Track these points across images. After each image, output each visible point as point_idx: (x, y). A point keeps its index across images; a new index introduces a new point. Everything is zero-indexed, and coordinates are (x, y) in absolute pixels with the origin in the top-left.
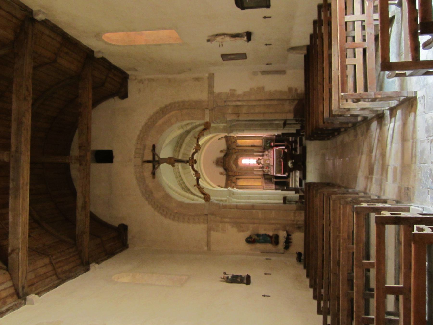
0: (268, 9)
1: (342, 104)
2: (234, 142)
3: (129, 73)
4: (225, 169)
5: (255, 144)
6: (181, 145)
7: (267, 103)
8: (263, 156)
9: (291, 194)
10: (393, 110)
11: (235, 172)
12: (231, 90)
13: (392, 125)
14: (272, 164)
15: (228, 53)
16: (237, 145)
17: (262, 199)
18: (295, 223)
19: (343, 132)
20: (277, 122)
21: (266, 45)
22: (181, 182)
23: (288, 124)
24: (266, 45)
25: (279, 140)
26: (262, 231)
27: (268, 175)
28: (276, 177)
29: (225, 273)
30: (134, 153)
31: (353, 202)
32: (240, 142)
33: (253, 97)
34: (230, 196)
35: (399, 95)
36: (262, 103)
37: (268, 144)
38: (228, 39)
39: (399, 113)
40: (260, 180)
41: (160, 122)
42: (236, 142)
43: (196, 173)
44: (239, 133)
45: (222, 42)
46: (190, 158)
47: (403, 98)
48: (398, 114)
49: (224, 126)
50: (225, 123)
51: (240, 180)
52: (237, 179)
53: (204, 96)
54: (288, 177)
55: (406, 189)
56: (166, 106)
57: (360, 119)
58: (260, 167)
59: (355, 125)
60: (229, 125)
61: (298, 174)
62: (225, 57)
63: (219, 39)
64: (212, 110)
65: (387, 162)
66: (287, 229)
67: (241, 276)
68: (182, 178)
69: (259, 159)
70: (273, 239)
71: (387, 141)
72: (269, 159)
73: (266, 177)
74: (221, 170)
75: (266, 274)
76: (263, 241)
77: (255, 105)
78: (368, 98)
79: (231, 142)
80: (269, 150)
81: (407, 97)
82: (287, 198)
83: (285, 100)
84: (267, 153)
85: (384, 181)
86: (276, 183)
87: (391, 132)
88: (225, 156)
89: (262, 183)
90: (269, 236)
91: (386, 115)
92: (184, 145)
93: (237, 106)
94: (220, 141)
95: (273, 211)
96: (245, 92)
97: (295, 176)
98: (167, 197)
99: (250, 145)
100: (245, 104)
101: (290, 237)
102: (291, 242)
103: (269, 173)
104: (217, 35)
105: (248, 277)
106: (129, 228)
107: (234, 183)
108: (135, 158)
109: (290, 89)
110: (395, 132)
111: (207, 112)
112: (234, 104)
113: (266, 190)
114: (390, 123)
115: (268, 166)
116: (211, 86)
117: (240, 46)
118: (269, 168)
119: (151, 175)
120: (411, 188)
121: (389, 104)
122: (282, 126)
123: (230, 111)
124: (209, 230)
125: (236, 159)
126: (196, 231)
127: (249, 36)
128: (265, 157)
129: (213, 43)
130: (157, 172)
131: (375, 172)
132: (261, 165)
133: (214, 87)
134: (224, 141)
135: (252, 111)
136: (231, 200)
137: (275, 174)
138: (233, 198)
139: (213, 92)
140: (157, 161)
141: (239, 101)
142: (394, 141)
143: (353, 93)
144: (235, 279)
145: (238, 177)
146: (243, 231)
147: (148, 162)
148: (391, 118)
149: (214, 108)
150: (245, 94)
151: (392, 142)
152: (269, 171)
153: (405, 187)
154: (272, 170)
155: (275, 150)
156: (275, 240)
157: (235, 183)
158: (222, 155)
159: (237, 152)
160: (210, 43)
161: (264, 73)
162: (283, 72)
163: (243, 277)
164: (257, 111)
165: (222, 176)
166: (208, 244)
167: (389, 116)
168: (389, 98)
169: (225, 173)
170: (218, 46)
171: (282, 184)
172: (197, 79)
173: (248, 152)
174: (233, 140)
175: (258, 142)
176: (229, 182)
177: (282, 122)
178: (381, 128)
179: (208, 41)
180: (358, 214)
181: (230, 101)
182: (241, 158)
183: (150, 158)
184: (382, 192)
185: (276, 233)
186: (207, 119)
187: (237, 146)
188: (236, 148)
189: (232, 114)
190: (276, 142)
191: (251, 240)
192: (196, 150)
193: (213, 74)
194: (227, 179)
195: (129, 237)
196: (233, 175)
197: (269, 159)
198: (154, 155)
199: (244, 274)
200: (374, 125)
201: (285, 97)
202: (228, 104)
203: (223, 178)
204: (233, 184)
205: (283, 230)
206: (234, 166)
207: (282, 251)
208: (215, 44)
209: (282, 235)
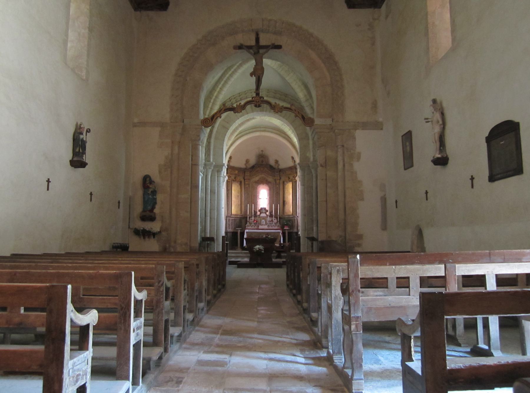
0: (487, 178)
1: (338, 271)
2: (289, 178)
3: (384, 6)
4: (253, 167)
5: (286, 206)
7: (341, 206)
8: (271, 216)
9: (218, 247)
10: (329, 360)
11: (249, 179)
12: (359, 154)
13: (303, 360)
14: (260, 227)
15: (413, 143)
16: (286, 183)
18: (172, 244)
19: (297, 299)
20: (315, 228)
21: (427, 193)
23: (312, 244)
24: (427, 193)
25: (292, 237)
26: (159, 197)
27: (246, 223)
28: (242, 234)
29: (88, 131)
30: (269, 18)
31: (160, 287)
32: (290, 186)
34: (215, 166)
35: (355, 365)
37: (287, 223)
38: (437, 129)
39: (321, 370)
40: (239, 213)
41: (313, 55)
42: (290, 181)
43: (243, 107)
44: (300, 183)
45: (432, 121)
46: (263, 98)
47: (350, 374)
48: (320, 368)
50: (314, 158)
51: (239, 187)
53: (351, 115)
54: (243, 248)
55: (180, 380)
56: (336, 63)
57: (314, 315)
58: (255, 213)
59: (306, 311)
60: (311, 165)
61: (247, 260)
62: (408, 137)
63: (438, 116)
64: (331, 128)
65: (238, 353)
66: (163, 233)
67: (84, 153)
69: (267, 211)
70: (148, 214)
71: (275, 353)
72: (266, 224)
73: (243, 221)
75: (91, 194)
76: (146, 199)
77: (337, 188)
78: (349, 310)
79: (290, 174)
80: (278, 224)
81: (352, 379)
82: (212, 243)
83: (345, 230)
84: (275, 221)
85: (206, 349)
86: (234, 234)
87: (289, 358)
88: (271, 167)
89: (236, 215)
90: (153, 208)
91: (319, 351)
93: (336, 163)
94: (291, 158)
95: (189, 215)
96: (356, 173)
97: (243, 257)
98: (209, 67)
99: (286, 200)
100: (340, 174)
101: (152, 237)
102: (144, 238)
103: (248, 224)
104: (442, 114)
105: (83, 165)
106: (165, 12)
107: (235, 178)
108: (263, 20)
109: (360, 237)
110: (289, 364)
111: (329, 121)
112: (340, 159)
113: (226, 220)
114: (304, 358)
115: (257, 223)
116: (365, 126)
117: (425, 149)
118: (255, 224)
119: (238, 44)
120: (178, 387)
121: (339, 353)
122: (311, 236)
123: (329, 153)
124: (162, 125)
125: (267, 181)
126: (160, 105)
127: (442, 161)
128: (269, 219)
129: (432, 108)
130: (244, 54)
131: (225, 337)
132: (258, 213)
133: (363, 129)
134: (291, 164)
135: (329, 185)
136: (210, 169)
137: (246, 231)
138: (213, 170)
139: (356, 129)
140: (259, 52)
141: (344, 166)
142: (272, 363)
143: (360, 277)
144: (79, 145)
146: (160, 172)
147: (257, 40)
148: (313, 359)
149: (334, 132)
151: (271, 359)
152: (251, 224)
153: (183, 378)
154: (253, 227)
155: (279, 231)
156: (148, 216)
157: (235, 180)
158: (272, 162)
159: (276, 182)
160: (432, 103)
161: (384, 200)
162: (384, 226)
163: (82, 157)
164: (329, 191)
165: (244, 162)
166: (143, 124)
167: (318, 355)
168: (349, 349)
169: (249, 166)
170: (426, 117)
171: (233, 239)
172: (375, 106)
173: (277, 197)
174: (291, 177)
175: (289, 209)
176: (237, 172)
177: (315, 236)
178: (297, 345)
179: (434, 101)
180: (117, 277)
181: (344, 153)
182: (267, 187)
183: (262, 42)
184: (188, 346)
185: (158, 217)
187: (283, 182)
188: (281, 181)
189: (326, 157)
190: (289, 233)
191: (148, 182)
192: (274, 106)
193: (382, 129)
194: (240, 170)
195: (151, 13)
196: (246, 178)
197: (266, 224)
198: (267, 47)
199: (88, 158)
200: (305, 337)
201: (349, 229)
202: (339, 150)
203: (240, 163)
204: (233, 177)
205: (161, 228)
206: (257, 179)
207: (131, 227)
208: (428, 111)
209: (155, 226)
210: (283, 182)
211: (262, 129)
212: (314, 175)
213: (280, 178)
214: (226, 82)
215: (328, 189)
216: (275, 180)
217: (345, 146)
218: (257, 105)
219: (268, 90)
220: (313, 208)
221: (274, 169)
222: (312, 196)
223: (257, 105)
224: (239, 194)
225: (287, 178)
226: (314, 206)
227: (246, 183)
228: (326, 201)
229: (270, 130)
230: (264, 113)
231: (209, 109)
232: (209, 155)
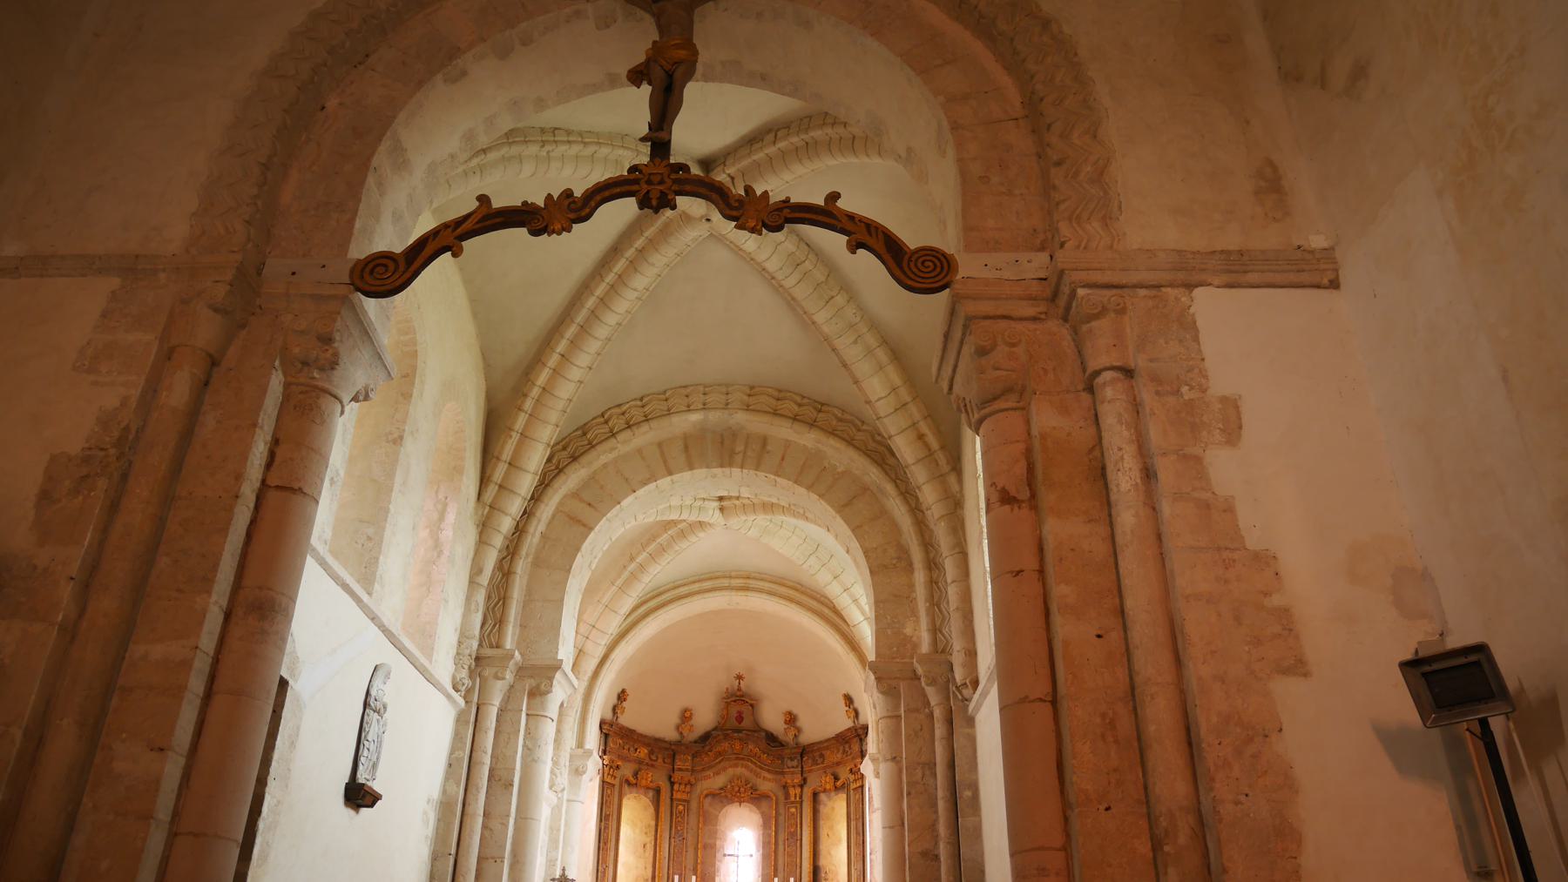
2: (836, 779)
4: (706, 737)
6: (812, 424)
12: (1232, 405)
16: (823, 797)
17: (481, 859)
22: (618, 423)
32: (836, 809)
33: (1191, 577)
36: (1152, 665)
49: (916, 646)
50: (935, 642)
51: (652, 810)
52: (658, 791)
60: (920, 671)
68: (638, 424)
74: (705, 719)
79: (838, 764)
88: (771, 738)
92: (809, 439)
94: (842, 702)
96: (1229, 509)
99: (822, 862)
100: (1128, 518)
107: (636, 775)
111: (1035, 264)
112: (1117, 437)
116: (1238, 270)
125: (754, 789)
134: (841, 722)
135: (1061, 591)
136: (497, 678)
139: (1190, 287)
141: (1149, 474)
145: (665, 796)
150: (1215, 513)
158: (772, 719)
159: (787, 796)
164: (1063, 627)
165: (674, 719)
174: (844, 774)
176: (643, 752)
181: (1136, 407)
186: (969, 267)
187: (815, 795)
188: (808, 791)
192: (740, 201)
193: (1334, 284)
194: (655, 745)
196: (677, 776)
203: (654, 718)
204: (627, 771)
206: (719, 781)
210: (815, 795)
211: (735, 582)
212: (938, 713)
213: (805, 780)
214: (584, 330)
215: (1058, 620)
216: (785, 787)
217: (1140, 362)
218: (654, 195)
219: (752, 388)
220: (937, 857)
221: (782, 745)
222: (935, 805)
223: (654, 195)
224: (650, 839)
225: (830, 779)
226: (943, 850)
227: (677, 796)
228: (1054, 702)
229: (767, 585)
230: (736, 471)
231: (515, 436)
232: (500, 622)
